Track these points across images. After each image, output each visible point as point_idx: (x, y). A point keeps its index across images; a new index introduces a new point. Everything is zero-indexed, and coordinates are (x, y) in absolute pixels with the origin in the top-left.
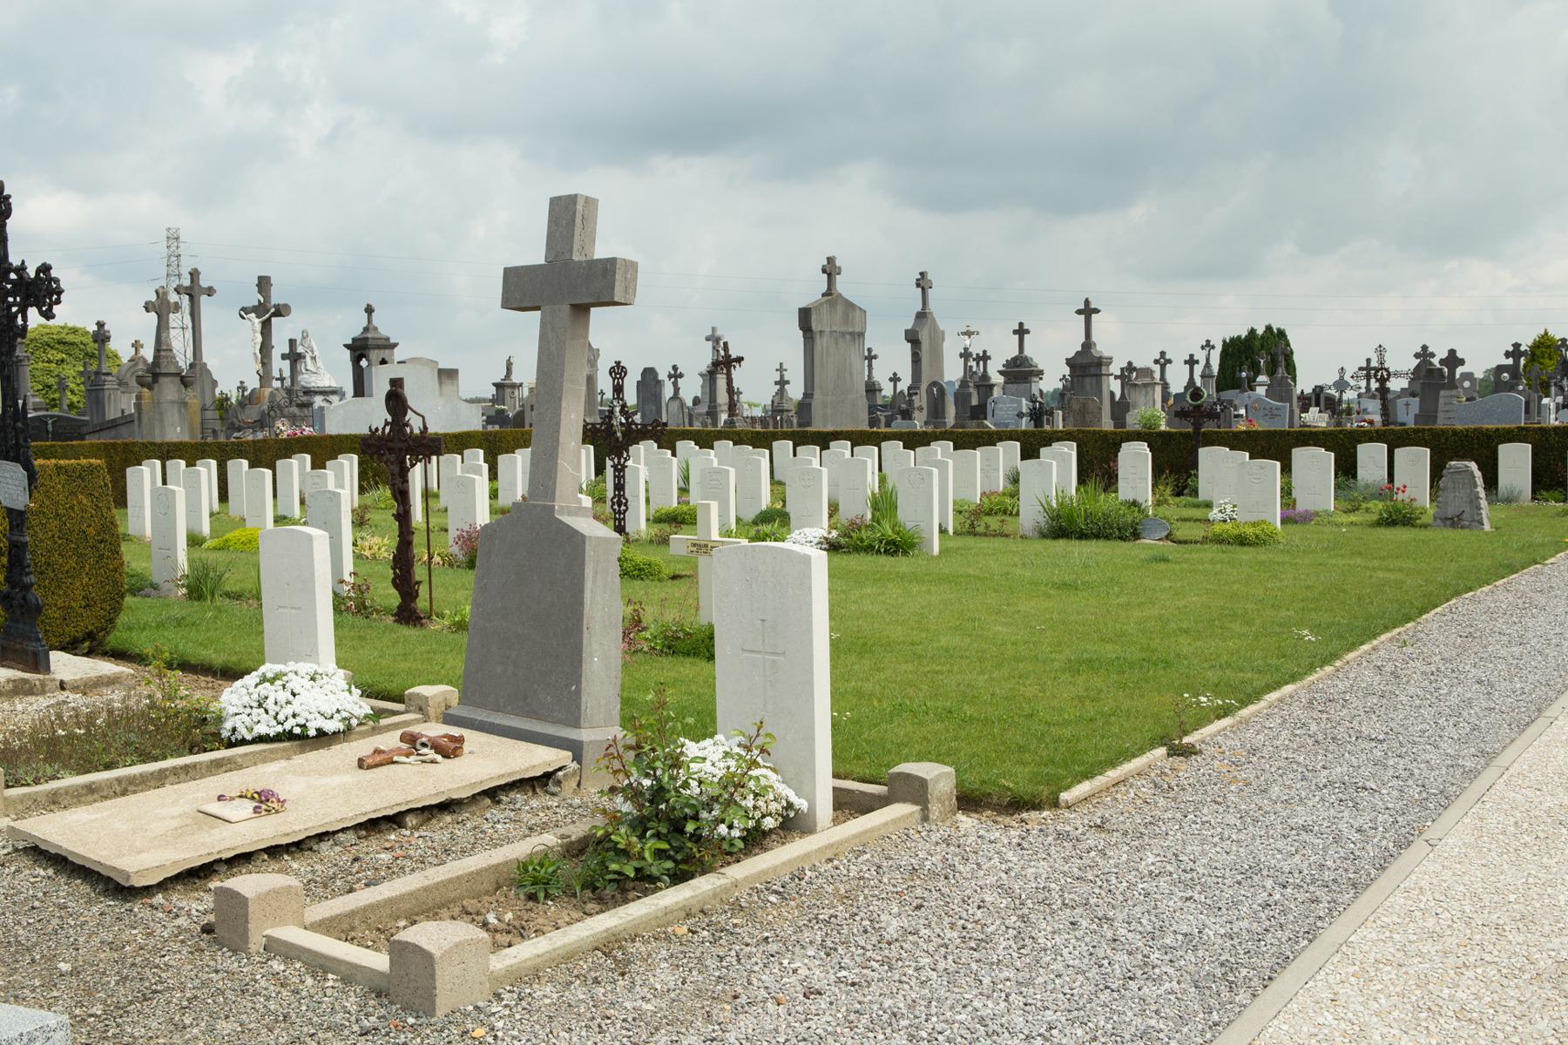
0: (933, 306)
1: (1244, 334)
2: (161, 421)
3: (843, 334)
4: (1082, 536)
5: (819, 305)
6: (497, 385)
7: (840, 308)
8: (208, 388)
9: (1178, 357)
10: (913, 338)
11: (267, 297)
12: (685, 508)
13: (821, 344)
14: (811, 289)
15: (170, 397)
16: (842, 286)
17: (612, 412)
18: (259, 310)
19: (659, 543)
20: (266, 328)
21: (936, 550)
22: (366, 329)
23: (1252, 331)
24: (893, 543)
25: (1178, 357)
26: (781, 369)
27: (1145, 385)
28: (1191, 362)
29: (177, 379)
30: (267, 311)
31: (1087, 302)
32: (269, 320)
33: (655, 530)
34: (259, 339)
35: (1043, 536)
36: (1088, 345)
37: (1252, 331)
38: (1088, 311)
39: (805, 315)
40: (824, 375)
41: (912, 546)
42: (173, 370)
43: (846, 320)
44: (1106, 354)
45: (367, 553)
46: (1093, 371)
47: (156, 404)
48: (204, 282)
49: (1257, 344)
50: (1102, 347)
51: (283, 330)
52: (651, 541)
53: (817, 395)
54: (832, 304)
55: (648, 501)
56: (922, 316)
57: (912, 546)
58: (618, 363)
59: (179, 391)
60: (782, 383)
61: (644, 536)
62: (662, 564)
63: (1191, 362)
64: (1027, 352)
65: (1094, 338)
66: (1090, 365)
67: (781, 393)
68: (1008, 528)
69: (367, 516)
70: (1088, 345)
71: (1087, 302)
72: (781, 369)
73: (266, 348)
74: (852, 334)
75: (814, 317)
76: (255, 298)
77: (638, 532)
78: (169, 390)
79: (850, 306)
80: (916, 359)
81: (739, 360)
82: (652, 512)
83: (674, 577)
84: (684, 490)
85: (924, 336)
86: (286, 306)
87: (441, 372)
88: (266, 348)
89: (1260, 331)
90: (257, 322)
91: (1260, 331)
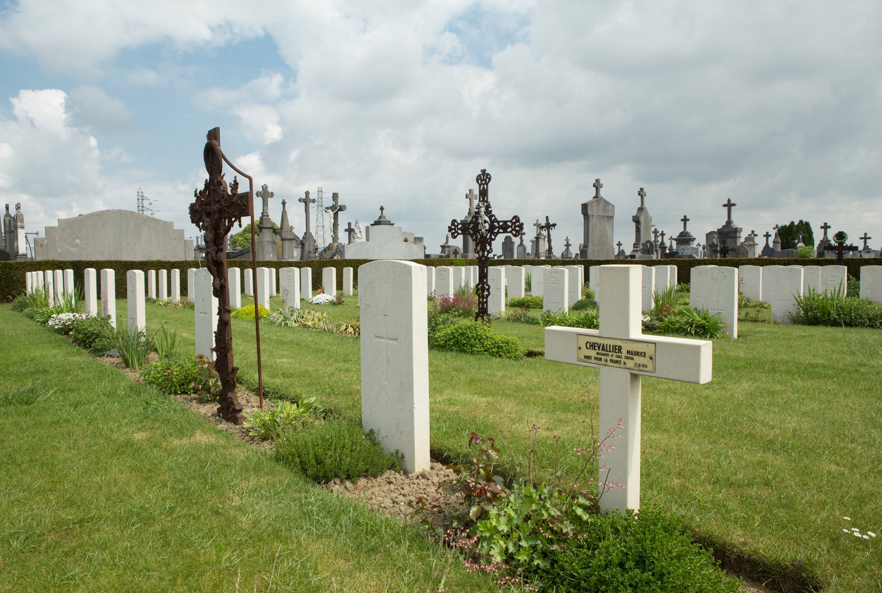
0: (646, 205)
1: (788, 224)
2: (263, 251)
3: (603, 217)
4: (835, 324)
5: (592, 202)
6: (443, 247)
7: (602, 204)
8: (312, 243)
9: (760, 233)
10: (636, 220)
11: (336, 202)
12: (530, 298)
13: (592, 221)
14: (588, 196)
15: (267, 239)
16: (603, 193)
17: (478, 213)
18: (333, 208)
19: (514, 321)
20: (336, 216)
21: (735, 335)
22: (380, 217)
23: (792, 223)
24: (703, 327)
25: (760, 233)
26: (567, 240)
27: (750, 245)
28: (767, 236)
29: (271, 231)
30: (337, 209)
31: (729, 200)
32: (337, 213)
33: (512, 311)
34: (333, 221)
35: (796, 321)
36: (729, 222)
37: (792, 223)
38: (729, 205)
39: (585, 207)
40: (594, 237)
41: (717, 329)
42: (269, 226)
43: (605, 210)
44: (739, 226)
45: (310, 323)
46: (732, 235)
47: (261, 242)
48: (311, 197)
49: (795, 229)
50: (736, 223)
51: (344, 219)
52: (508, 319)
53: (590, 246)
54: (598, 202)
55: (506, 294)
56: (641, 209)
57: (717, 329)
58: (484, 171)
59: (272, 236)
60: (568, 245)
61: (503, 315)
62: (519, 342)
63: (767, 236)
64: (688, 230)
65: (732, 219)
66: (731, 232)
67: (567, 249)
68: (761, 316)
69: (343, 299)
70: (729, 222)
71: (729, 200)
72: (567, 240)
73: (335, 225)
74: (608, 217)
75: (589, 208)
76: (331, 203)
77: (500, 313)
78: (267, 236)
79: (607, 203)
80: (638, 231)
81: (554, 225)
82: (509, 300)
83: (530, 354)
84: (529, 285)
85: (642, 219)
86: (344, 206)
87: (415, 238)
88: (335, 225)
89: (796, 223)
90: (332, 213)
91: (796, 223)
